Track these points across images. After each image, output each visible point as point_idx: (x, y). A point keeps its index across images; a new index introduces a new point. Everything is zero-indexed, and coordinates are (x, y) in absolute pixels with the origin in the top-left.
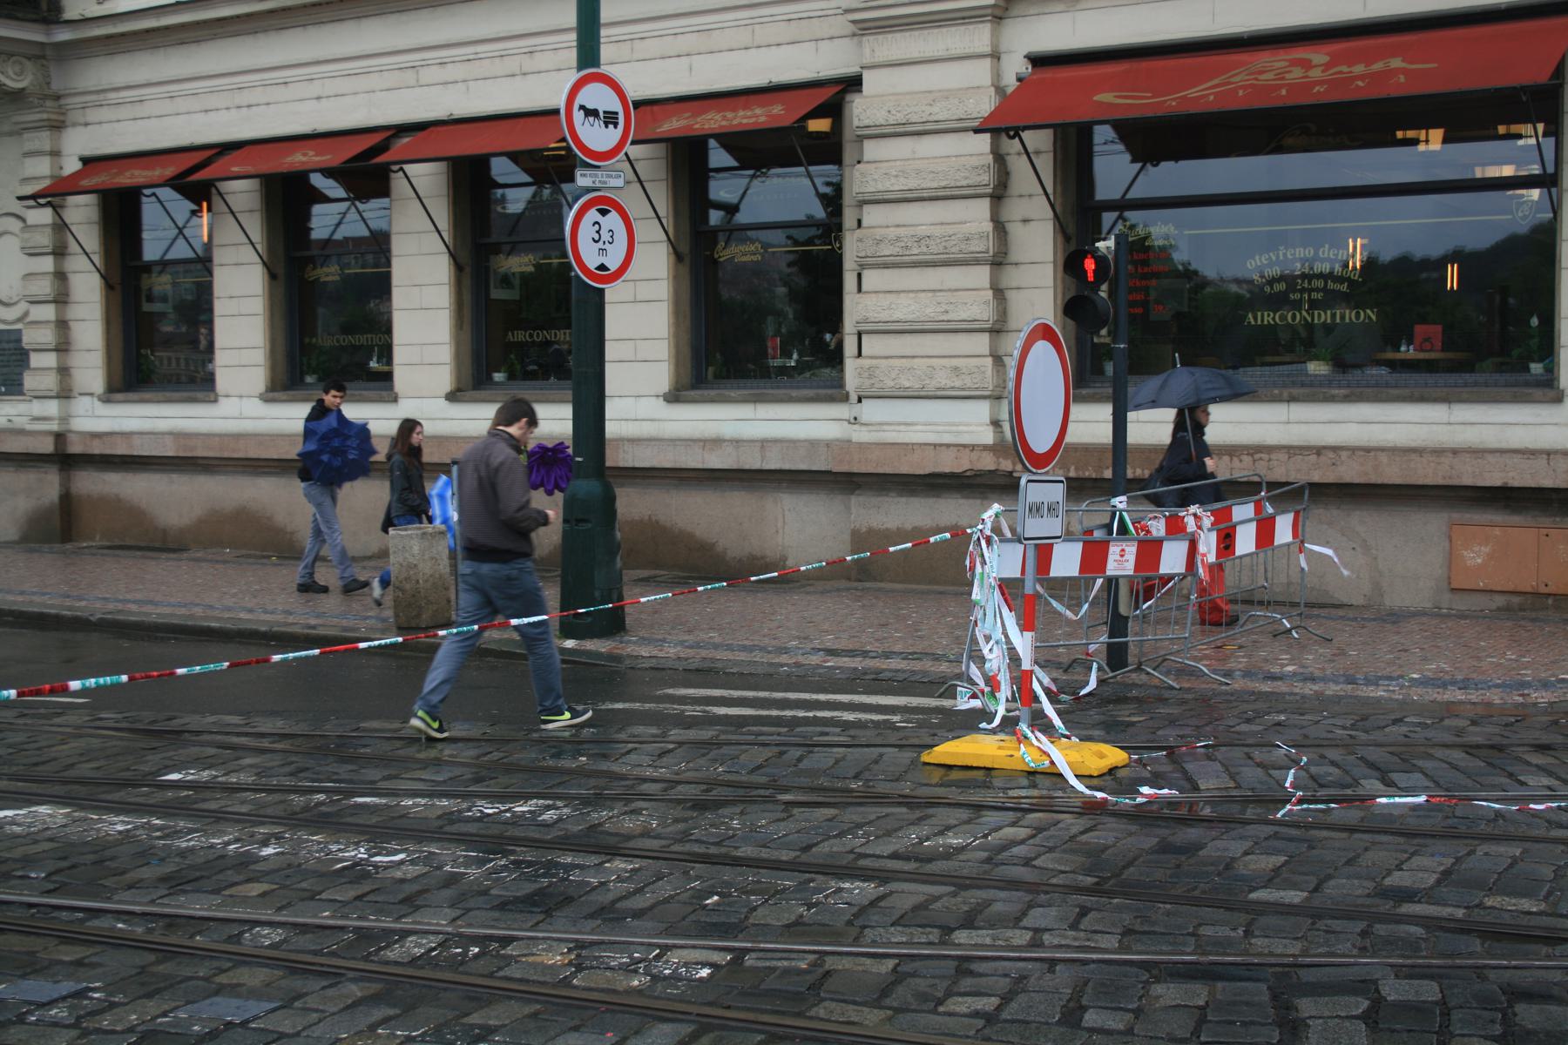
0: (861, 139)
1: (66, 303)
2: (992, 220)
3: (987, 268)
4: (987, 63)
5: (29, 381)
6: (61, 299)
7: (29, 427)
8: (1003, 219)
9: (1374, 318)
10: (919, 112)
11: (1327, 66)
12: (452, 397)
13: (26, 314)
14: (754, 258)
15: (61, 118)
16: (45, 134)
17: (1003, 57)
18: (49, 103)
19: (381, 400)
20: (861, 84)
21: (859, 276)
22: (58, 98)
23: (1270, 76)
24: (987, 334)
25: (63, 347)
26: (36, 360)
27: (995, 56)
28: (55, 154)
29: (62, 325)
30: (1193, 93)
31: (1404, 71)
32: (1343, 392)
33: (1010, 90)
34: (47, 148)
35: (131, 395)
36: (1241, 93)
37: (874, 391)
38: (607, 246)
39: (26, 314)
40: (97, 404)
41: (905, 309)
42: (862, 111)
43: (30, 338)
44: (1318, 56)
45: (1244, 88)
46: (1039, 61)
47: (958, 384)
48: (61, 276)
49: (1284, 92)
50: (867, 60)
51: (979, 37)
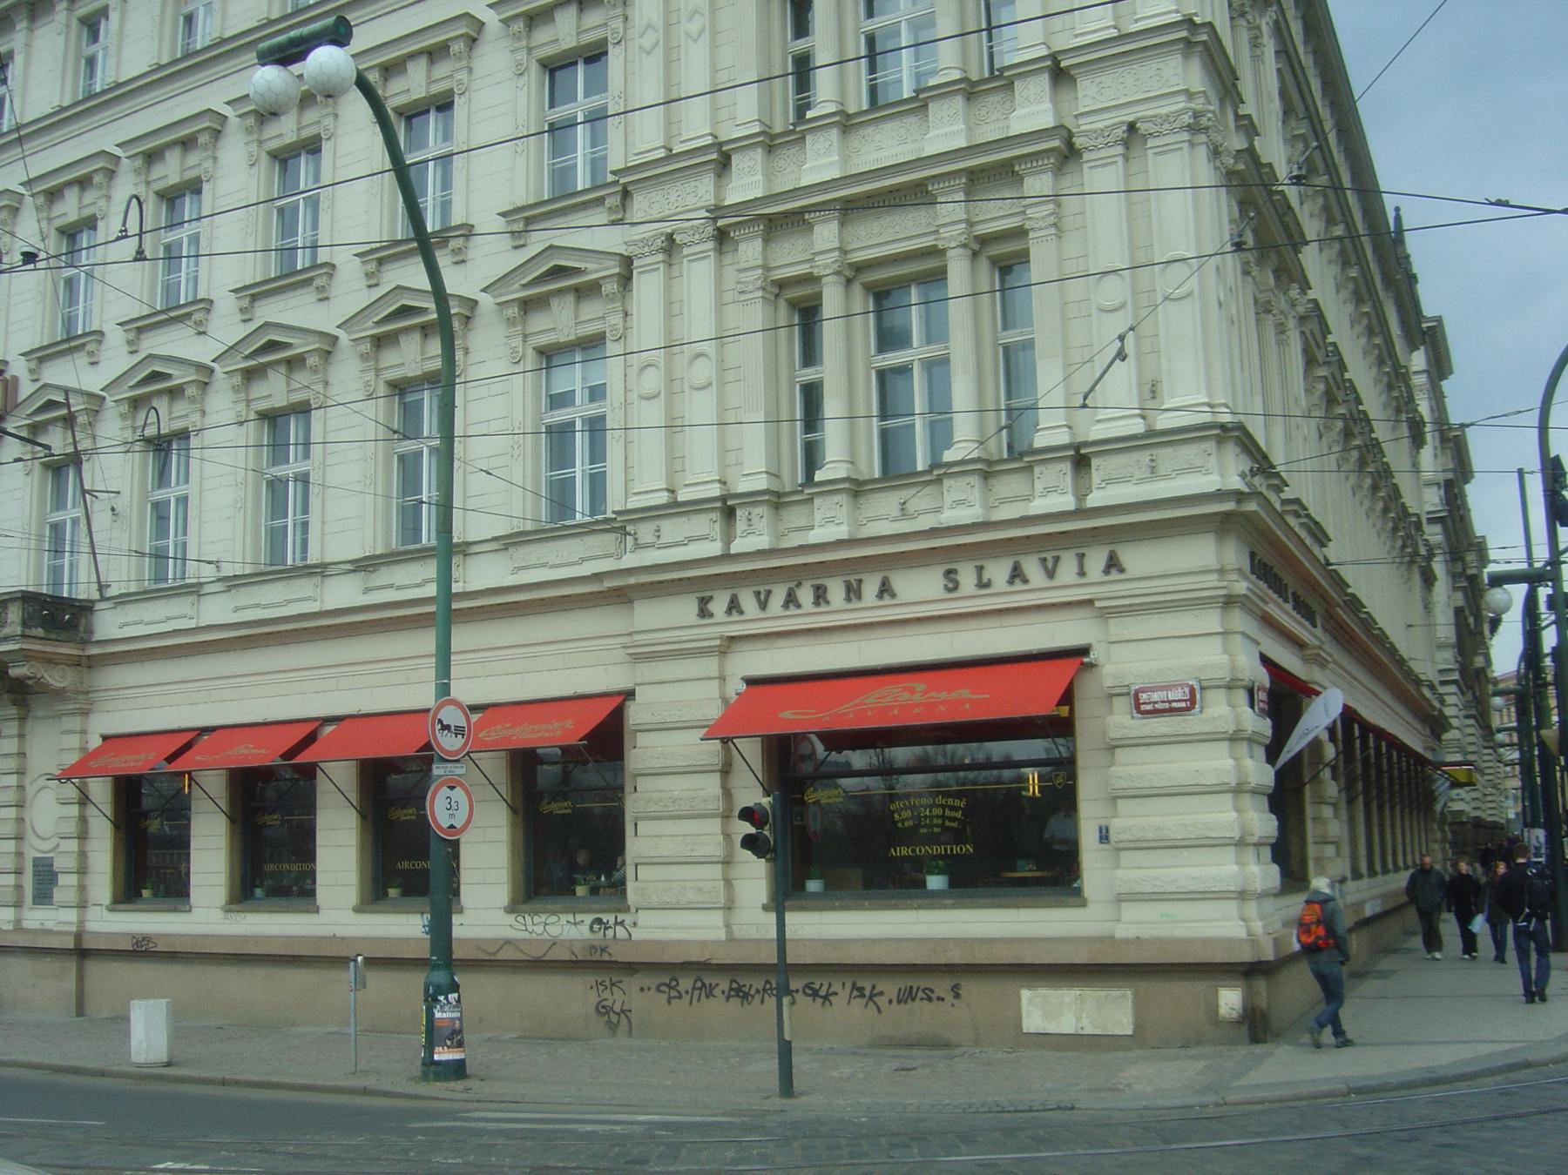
0: (636, 731)
1: (85, 838)
2: (722, 787)
3: (720, 820)
4: (717, 682)
5: (58, 895)
6: (83, 836)
7: (55, 929)
8: (729, 786)
9: (971, 850)
10: (674, 716)
11: (925, 693)
12: (358, 910)
13: (58, 845)
14: (566, 811)
15: (89, 707)
16: (78, 719)
17: (728, 678)
18: (81, 697)
19: (308, 911)
20: (634, 695)
21: (636, 824)
22: (88, 693)
23: (889, 699)
24: (720, 866)
25: (82, 870)
26: (62, 879)
27: (722, 678)
28: (83, 732)
29: (83, 855)
30: (841, 710)
31: (969, 701)
32: (951, 901)
33: (732, 701)
34: (78, 728)
35: (129, 906)
36: (870, 713)
37: (645, 905)
38: (455, 812)
39: (58, 845)
40: (105, 912)
41: (666, 849)
42: (635, 715)
43: (58, 865)
44: (919, 685)
45: (872, 709)
46: (751, 682)
47: (701, 899)
48: (83, 820)
49: (896, 712)
50: (639, 681)
51: (710, 666)
